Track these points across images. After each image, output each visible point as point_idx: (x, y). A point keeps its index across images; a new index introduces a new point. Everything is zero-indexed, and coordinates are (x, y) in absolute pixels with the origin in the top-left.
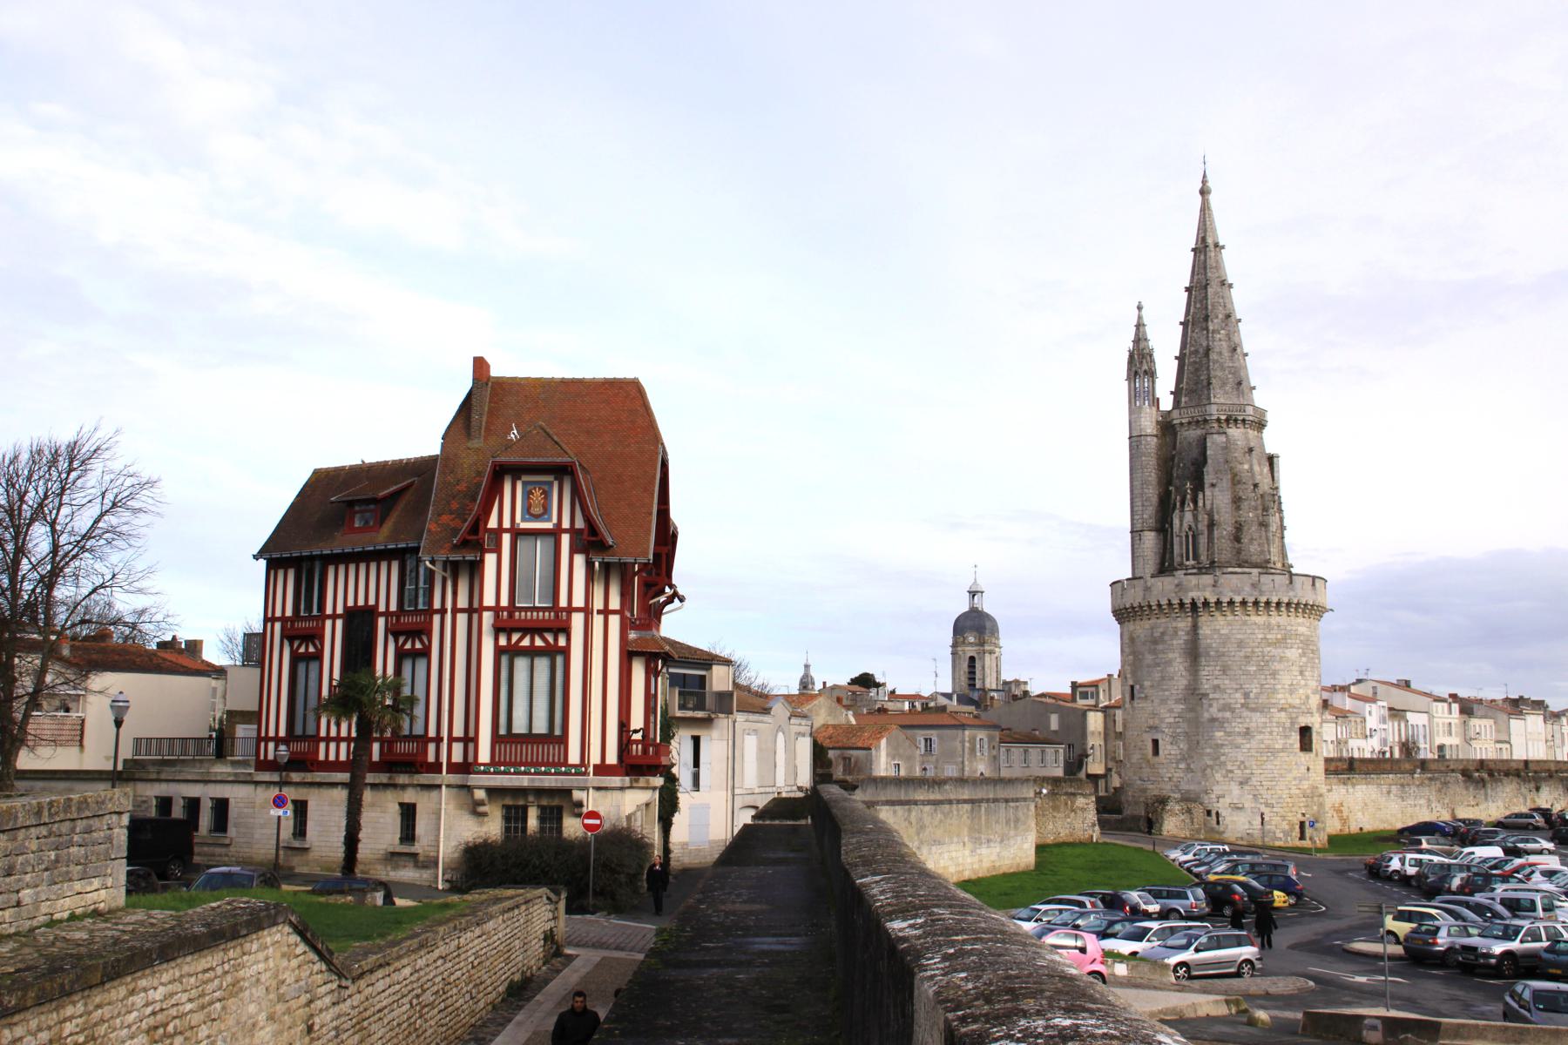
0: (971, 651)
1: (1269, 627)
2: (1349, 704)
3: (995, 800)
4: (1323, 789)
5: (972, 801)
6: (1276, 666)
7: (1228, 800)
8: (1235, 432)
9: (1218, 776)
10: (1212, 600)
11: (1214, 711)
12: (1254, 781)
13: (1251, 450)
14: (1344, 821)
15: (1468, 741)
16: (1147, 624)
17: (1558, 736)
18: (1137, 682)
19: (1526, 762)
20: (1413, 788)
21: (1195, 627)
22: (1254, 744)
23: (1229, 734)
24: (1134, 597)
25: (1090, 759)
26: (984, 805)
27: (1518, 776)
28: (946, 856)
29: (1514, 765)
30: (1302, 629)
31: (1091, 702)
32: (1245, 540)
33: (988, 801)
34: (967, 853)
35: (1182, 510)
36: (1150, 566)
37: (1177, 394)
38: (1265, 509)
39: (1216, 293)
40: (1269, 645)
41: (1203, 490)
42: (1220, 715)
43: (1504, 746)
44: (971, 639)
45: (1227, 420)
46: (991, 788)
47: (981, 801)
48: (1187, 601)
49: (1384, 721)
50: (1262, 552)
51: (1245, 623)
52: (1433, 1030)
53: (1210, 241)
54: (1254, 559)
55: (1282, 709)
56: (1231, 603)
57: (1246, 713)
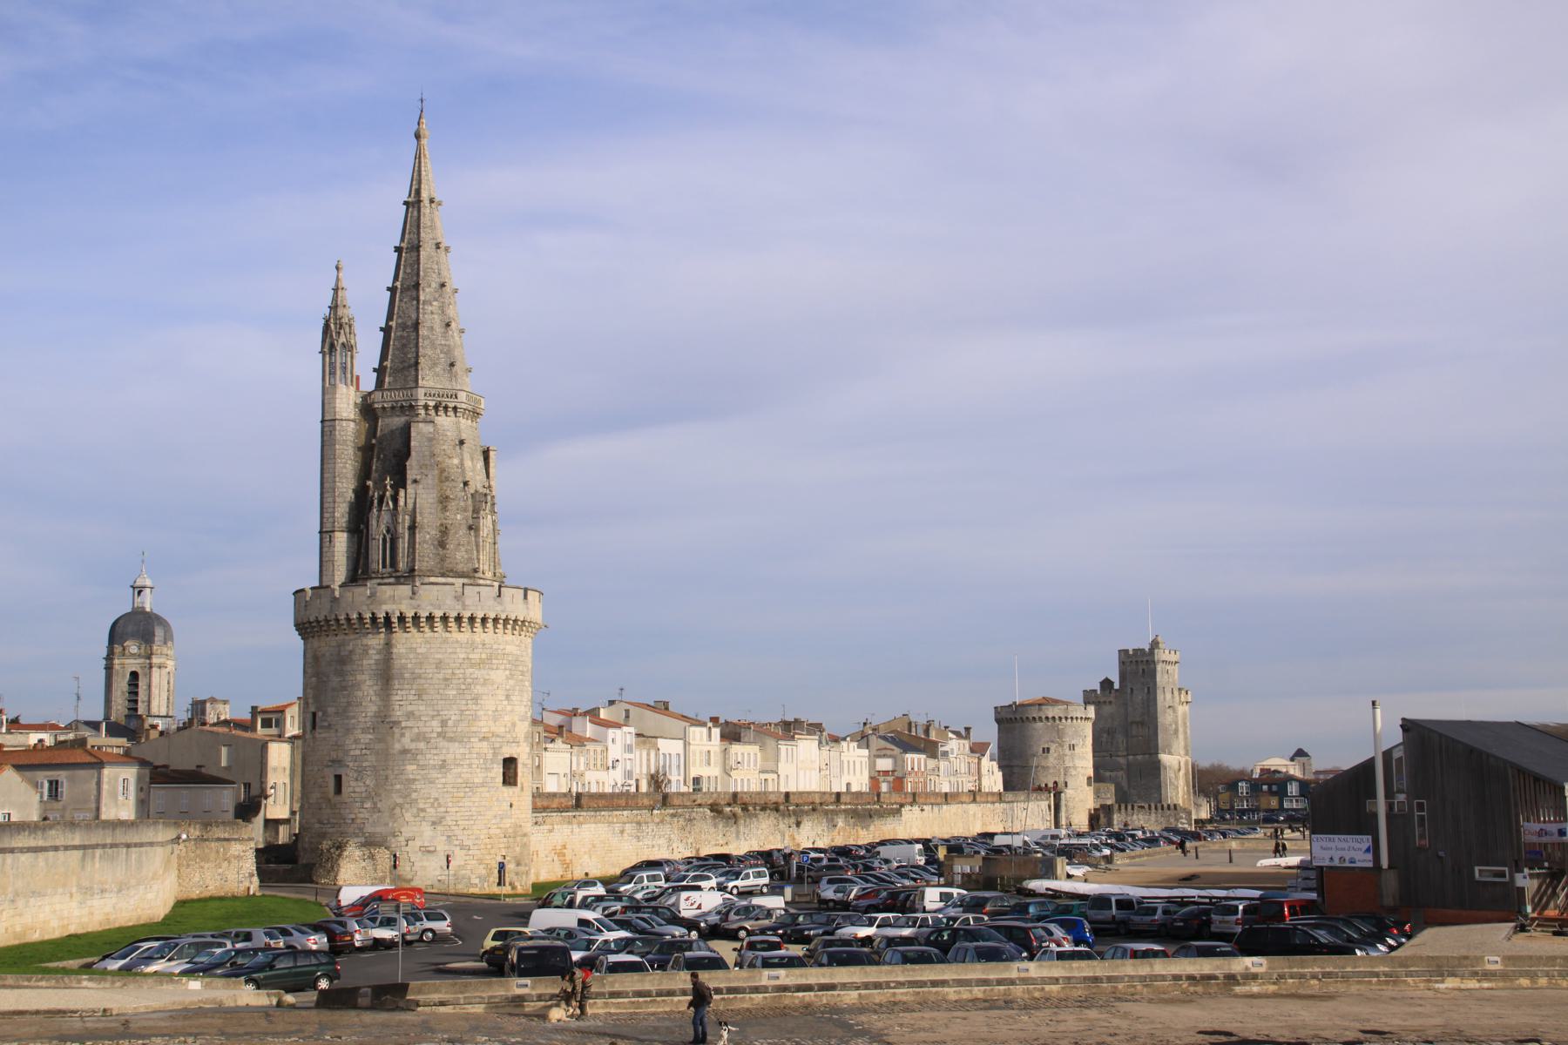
0: (133, 664)
1: (473, 646)
2: (590, 730)
3: (113, 846)
4: (528, 827)
5: (84, 847)
6: (478, 689)
7: (418, 843)
8: (444, 421)
9: (408, 816)
10: (410, 614)
11: (406, 742)
12: (449, 820)
13: (462, 442)
14: (567, 866)
15: (727, 772)
16: (333, 641)
17: (835, 764)
18: (319, 709)
19: (787, 795)
20: (651, 826)
21: (388, 645)
22: (450, 778)
23: (423, 767)
24: (320, 611)
25: (271, 800)
26: (98, 852)
27: (777, 810)
28: (47, 909)
29: (773, 798)
30: (509, 648)
31: (274, 731)
32: (451, 546)
33: (104, 846)
34: (74, 904)
35: (380, 510)
36: (340, 574)
37: (380, 371)
38: (476, 511)
39: (430, 257)
40: (472, 665)
41: (404, 487)
42: (413, 746)
43: (770, 776)
44: (134, 649)
45: (436, 408)
46: (109, 832)
47: (96, 846)
48: (381, 615)
49: (629, 749)
50: (470, 559)
51: (445, 641)
52: (461, 1041)
53: (425, 195)
54: (461, 567)
55: (484, 739)
56: (430, 618)
57: (443, 743)
